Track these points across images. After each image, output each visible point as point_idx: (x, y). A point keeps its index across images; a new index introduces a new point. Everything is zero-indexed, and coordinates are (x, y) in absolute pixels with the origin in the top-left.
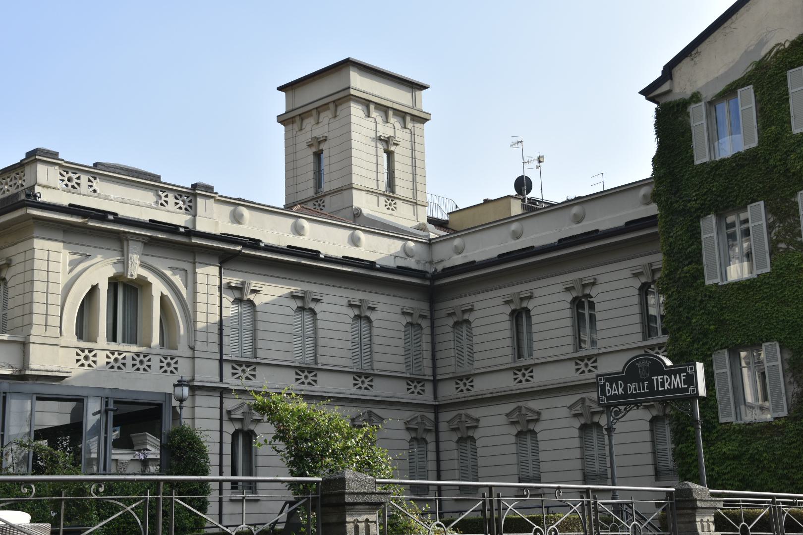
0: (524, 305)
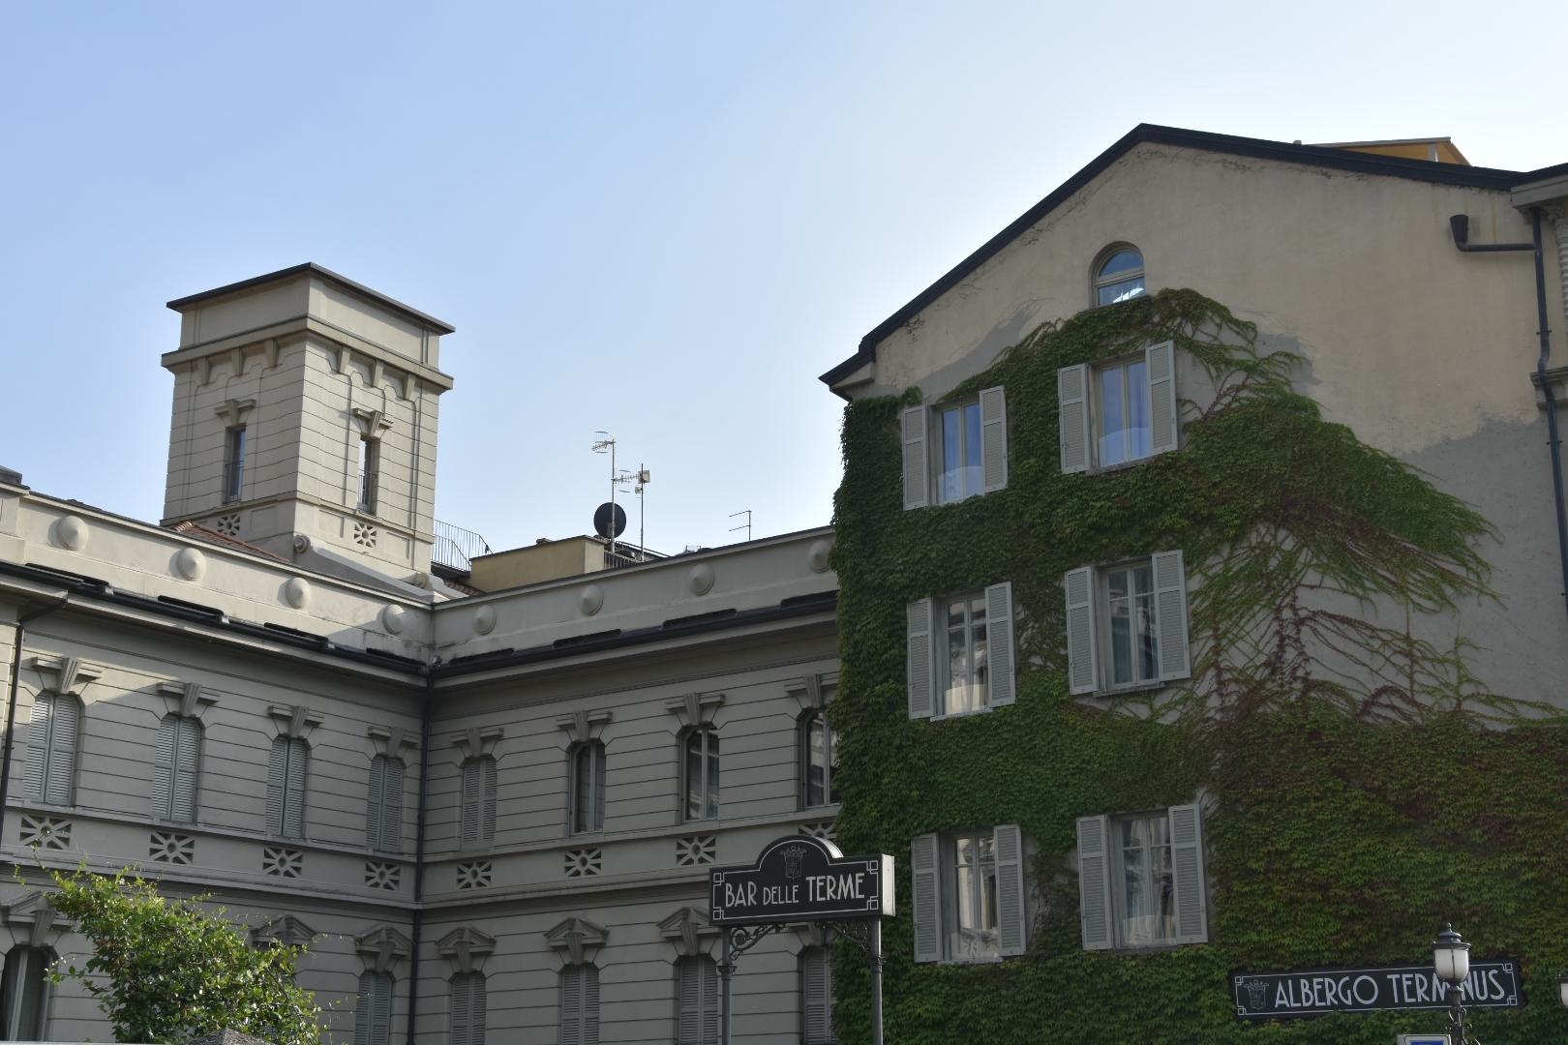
0: (595, 735)
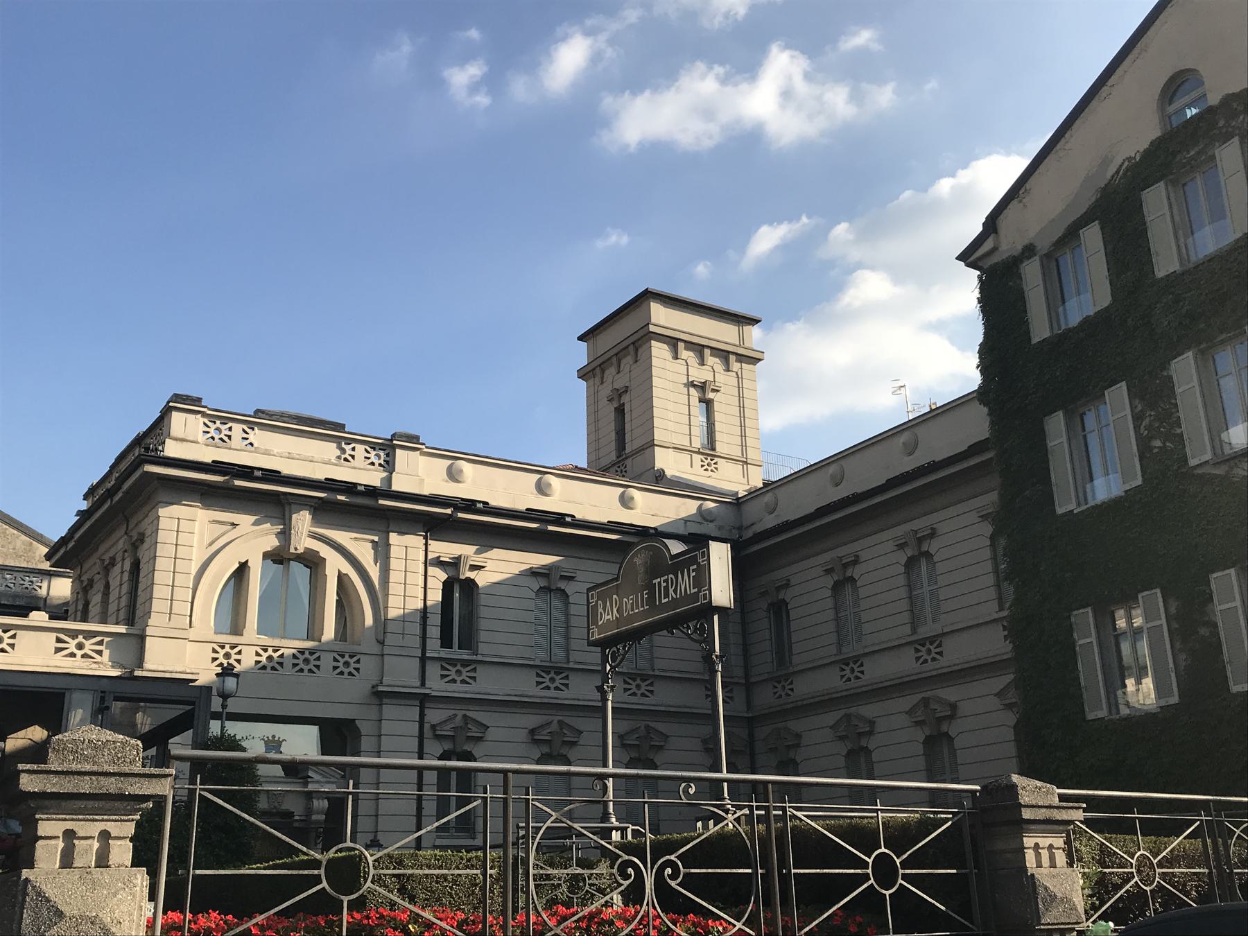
0: (849, 574)
